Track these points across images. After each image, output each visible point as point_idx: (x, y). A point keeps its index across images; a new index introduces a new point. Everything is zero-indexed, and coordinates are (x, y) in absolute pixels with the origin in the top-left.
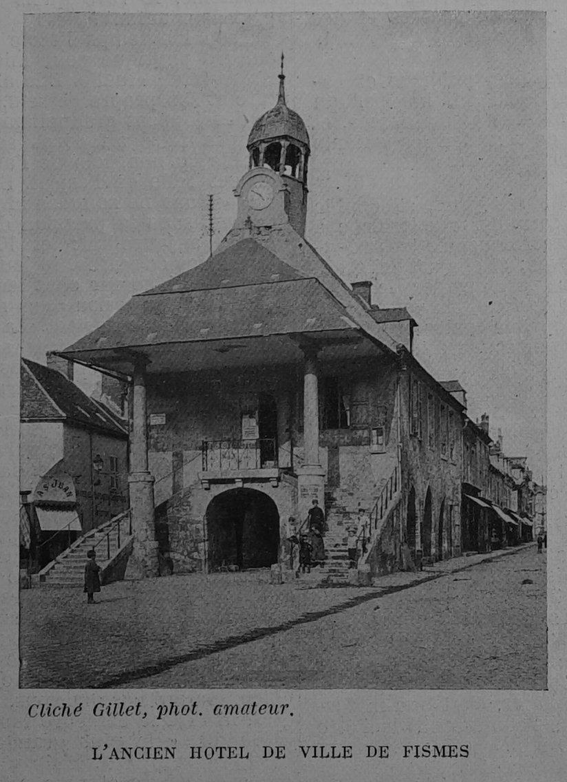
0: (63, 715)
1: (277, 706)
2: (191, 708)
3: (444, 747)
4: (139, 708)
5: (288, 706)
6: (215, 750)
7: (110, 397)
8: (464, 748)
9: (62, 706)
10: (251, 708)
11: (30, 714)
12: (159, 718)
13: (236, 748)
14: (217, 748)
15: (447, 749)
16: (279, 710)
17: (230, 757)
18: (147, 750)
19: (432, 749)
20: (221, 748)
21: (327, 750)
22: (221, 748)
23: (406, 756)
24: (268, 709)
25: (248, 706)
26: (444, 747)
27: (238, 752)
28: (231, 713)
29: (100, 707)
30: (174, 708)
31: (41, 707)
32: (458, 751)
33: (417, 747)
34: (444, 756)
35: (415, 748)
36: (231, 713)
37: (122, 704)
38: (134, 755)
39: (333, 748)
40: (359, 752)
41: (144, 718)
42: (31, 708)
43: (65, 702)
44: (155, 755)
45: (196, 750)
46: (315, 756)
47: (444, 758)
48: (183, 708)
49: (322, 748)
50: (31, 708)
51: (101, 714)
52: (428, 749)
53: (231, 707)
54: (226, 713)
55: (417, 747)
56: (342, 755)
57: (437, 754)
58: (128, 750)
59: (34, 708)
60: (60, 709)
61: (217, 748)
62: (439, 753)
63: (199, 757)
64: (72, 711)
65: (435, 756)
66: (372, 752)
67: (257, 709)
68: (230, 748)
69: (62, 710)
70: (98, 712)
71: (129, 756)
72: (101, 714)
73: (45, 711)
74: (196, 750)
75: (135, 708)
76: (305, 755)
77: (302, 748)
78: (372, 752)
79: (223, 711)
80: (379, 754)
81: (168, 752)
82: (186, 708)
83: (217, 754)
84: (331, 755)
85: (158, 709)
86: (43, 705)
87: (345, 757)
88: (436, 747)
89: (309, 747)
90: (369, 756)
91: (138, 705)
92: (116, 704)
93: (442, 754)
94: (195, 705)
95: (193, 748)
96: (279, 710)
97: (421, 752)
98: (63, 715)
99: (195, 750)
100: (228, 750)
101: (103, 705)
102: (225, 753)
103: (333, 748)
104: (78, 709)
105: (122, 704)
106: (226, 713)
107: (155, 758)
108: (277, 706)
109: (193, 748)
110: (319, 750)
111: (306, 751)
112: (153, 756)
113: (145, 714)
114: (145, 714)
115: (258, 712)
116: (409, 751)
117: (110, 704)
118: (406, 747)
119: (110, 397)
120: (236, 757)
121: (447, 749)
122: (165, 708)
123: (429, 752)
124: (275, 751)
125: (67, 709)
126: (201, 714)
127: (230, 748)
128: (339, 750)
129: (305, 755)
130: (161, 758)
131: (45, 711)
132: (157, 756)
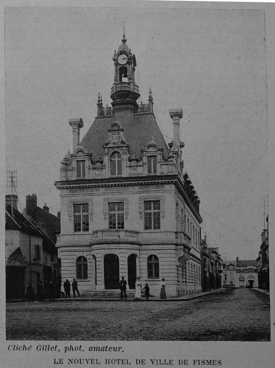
0: (23, 350)
1: (117, 347)
2: (79, 348)
3: (211, 361)
4: (57, 347)
5: (121, 348)
6: (116, 361)
7: (31, 217)
8: (219, 361)
9: (23, 346)
10: (105, 348)
11: (9, 349)
12: (65, 352)
13: (197, 360)
14: (117, 360)
15: (212, 362)
16: (118, 349)
17: (92, 363)
18: (91, 360)
19: (206, 362)
20: (118, 360)
21: (162, 361)
22: (118, 360)
23: (194, 364)
24: (113, 349)
25: (104, 347)
26: (211, 361)
27: (126, 362)
28: (96, 350)
29: (39, 347)
30: (72, 348)
31: (13, 346)
32: (217, 362)
33: (199, 361)
34: (211, 364)
35: (198, 361)
36: (96, 350)
37: (49, 346)
38: (74, 362)
39: (165, 360)
40: (191, 362)
41: (58, 352)
42: (9, 346)
43: (24, 344)
44: (92, 363)
45: (108, 360)
46: (157, 364)
47: (211, 365)
48: (75, 348)
49: (160, 360)
50: (9, 346)
51: (40, 350)
52: (202, 363)
53: (96, 348)
54: (94, 350)
55: (199, 361)
56: (59, 362)
57: (208, 364)
58: (71, 360)
59: (11, 347)
60: (22, 347)
61: (117, 360)
62: (209, 363)
63: (109, 363)
64: (27, 348)
65: (207, 365)
66: (138, 362)
67: (108, 349)
68: (122, 360)
69: (23, 347)
70: (39, 349)
71: (72, 363)
72: (40, 350)
73: (15, 348)
74: (108, 360)
75: (55, 348)
76: (153, 363)
77: (152, 360)
78: (138, 362)
79: (93, 349)
80: (141, 363)
81: (70, 361)
82: (77, 348)
83: (117, 362)
84: (164, 363)
85: (65, 348)
86: (15, 345)
87: (60, 363)
88: (207, 361)
89: (154, 360)
90: (137, 364)
91: (56, 346)
92: (46, 346)
93: (210, 364)
94: (80, 347)
95: (106, 360)
96: (118, 349)
97: (201, 363)
98: (23, 350)
99: (107, 361)
100: (121, 360)
101: (41, 346)
102: (120, 362)
103: (165, 360)
104: (30, 347)
105: (49, 346)
106: (94, 350)
107: (213, 364)
108: (117, 347)
109: (106, 360)
110: (159, 361)
111: (153, 362)
112: (213, 364)
113: (59, 350)
114: (59, 350)
115: (108, 350)
116: (196, 362)
117: (44, 345)
118: (194, 361)
119: (31, 217)
120: (94, 364)
121: (212, 362)
122: (68, 348)
123: (204, 363)
124: (141, 361)
125: (25, 348)
126: (83, 351)
127: (122, 360)
128: (167, 361)
129: (153, 363)
130: (94, 364)
131: (15, 348)
132: (186, 364)
